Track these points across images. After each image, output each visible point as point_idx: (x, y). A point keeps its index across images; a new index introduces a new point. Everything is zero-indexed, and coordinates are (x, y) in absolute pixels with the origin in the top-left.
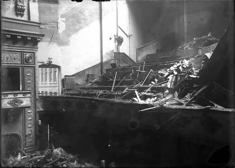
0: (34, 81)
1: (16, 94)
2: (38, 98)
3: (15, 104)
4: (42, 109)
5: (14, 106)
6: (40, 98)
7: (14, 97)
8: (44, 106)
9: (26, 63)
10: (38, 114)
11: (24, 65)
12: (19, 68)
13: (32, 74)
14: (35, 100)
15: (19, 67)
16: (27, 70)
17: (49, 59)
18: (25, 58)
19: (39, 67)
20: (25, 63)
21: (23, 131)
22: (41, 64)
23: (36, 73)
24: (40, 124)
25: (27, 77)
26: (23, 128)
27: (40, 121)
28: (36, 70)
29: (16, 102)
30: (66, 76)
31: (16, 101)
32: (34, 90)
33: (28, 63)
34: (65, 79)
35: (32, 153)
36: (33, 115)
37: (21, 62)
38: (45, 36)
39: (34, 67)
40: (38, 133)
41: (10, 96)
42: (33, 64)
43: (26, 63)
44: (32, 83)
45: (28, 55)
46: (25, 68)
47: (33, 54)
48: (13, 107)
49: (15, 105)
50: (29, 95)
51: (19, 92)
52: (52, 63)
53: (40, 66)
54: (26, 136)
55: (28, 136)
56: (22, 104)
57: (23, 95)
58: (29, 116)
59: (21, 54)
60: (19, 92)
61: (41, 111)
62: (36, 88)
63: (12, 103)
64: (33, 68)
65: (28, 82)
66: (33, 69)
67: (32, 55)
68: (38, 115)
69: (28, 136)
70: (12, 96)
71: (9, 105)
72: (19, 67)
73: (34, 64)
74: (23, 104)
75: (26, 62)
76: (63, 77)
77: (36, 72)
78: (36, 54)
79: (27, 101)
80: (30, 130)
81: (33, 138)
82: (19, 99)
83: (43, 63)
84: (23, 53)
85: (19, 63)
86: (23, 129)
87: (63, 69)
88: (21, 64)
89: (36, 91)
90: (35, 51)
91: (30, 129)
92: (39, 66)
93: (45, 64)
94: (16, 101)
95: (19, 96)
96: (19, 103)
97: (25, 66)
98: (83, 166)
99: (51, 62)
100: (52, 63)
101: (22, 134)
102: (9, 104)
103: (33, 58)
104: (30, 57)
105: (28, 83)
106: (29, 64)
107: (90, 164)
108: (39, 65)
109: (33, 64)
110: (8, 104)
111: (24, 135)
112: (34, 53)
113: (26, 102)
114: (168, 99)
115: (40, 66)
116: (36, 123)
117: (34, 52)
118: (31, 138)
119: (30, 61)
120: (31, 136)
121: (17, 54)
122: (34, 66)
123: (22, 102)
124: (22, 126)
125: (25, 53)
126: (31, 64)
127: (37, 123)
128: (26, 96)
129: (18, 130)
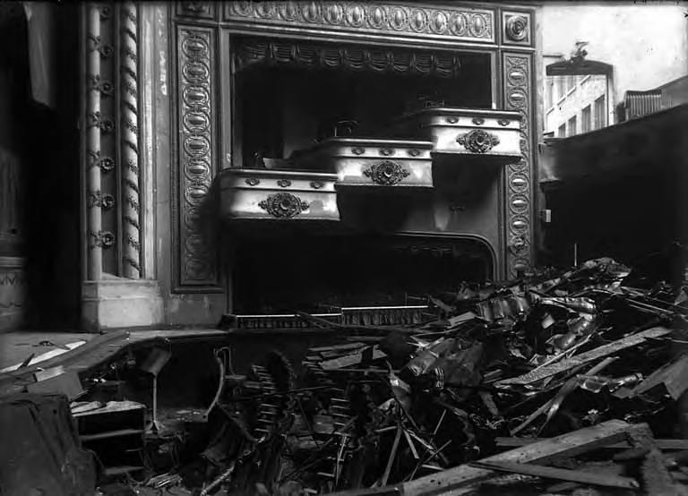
1: (481, 117)
2: (542, 144)
3: (478, 145)
4: (553, 178)
5: (474, 150)
6: (549, 143)
7: (475, 125)
9: (508, 42)
10: (543, 191)
11: (503, 47)
12: (488, 56)
13: (527, 96)
14: (536, 149)
15: (490, 52)
16: (509, 61)
17: (577, 44)
18: (506, 25)
20: (506, 41)
21: (500, 235)
24: (548, 219)
27: (548, 212)
29: (481, 139)
30: (629, 93)
34: (628, 103)
35: (520, 361)
36: (527, 191)
38: (509, 438)
39: (532, 53)
40: (542, 247)
41: (463, 122)
42: (529, 43)
43: (508, 42)
44: (526, 100)
46: (505, 54)
50: (515, 124)
51: (488, 112)
53: (551, 71)
54: (508, 250)
55: (514, 251)
57: (500, 123)
58: (517, 196)
60: (488, 112)
61: (550, 182)
62: (536, 129)
63: (470, 142)
64: (529, 56)
66: (529, 60)
67: (526, 18)
68: (541, 196)
69: (514, 251)
70: (467, 122)
72: (490, 52)
73: (533, 45)
74: (497, 150)
75: (509, 38)
76: (621, 98)
81: (528, 262)
82: (489, 132)
83: (560, 57)
84: (499, 12)
85: (490, 40)
88: (496, 43)
91: (520, 232)
92: (547, 67)
95: (296, 185)
96: (487, 143)
97: (506, 51)
98: (585, 325)
99: (585, 53)
100: (587, 58)
102: (461, 144)
103: (528, 28)
105: (514, 99)
108: (548, 64)
109: (529, 43)
111: (503, 247)
113: (508, 142)
115: (551, 71)
116: (537, 219)
118: (521, 258)
119: (522, 34)
121: (484, 16)
122: (530, 49)
123: (496, 143)
124: (496, 221)
125: (505, 13)
126: (525, 43)
127: (540, 217)
128: (507, 127)
129: (484, 229)
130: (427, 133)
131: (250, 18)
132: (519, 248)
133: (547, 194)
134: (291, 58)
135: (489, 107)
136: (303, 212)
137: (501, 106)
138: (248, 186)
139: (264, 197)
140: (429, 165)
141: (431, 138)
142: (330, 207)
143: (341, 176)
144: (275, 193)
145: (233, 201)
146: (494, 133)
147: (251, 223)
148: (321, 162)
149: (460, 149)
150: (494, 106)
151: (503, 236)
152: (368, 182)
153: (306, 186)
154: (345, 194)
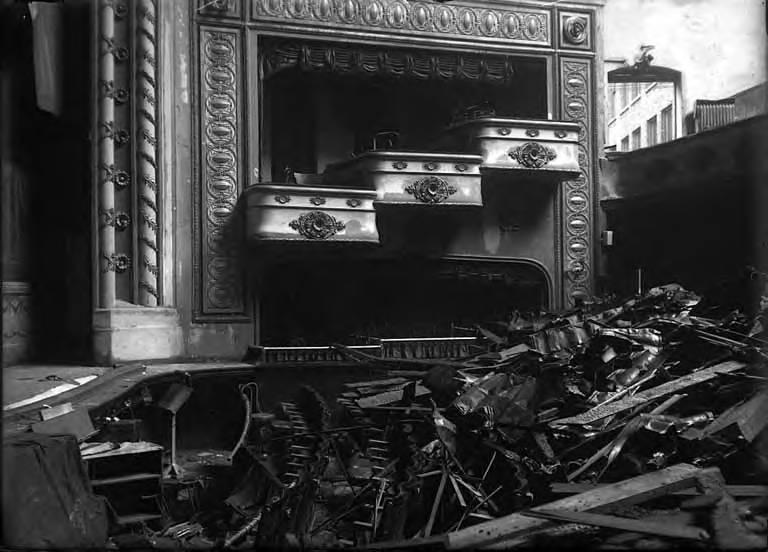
0: (591, 177)
1: (536, 129)
2: (603, 158)
6: (612, 158)
8: (621, 185)
9: (563, 45)
12: (544, 61)
17: (642, 48)
19: (610, 81)
21: (556, 260)
22: (613, 67)
23: (598, 79)
24: (610, 242)
25: (571, 113)
26: (556, 247)
27: (610, 233)
28: (597, 69)
30: (700, 102)
31: (532, 150)
32: (592, 111)
33: (572, 43)
34: (698, 113)
37: (549, 40)
39: (592, 58)
42: (589, 47)
45: (574, 17)
46: (562, 59)
47: (587, 16)
48: (524, 168)
49: (530, 162)
50: (574, 137)
52: (652, 63)
53: (613, 77)
54: (565, 275)
55: (572, 277)
56: (551, 163)
58: (576, 216)
59: (554, 58)
63: (306, 227)
64: (588, 61)
65: (572, 105)
67: (585, 19)
68: (601, 213)
69: (572, 277)
70: (520, 134)
71: (515, 162)
73: (593, 49)
75: (567, 40)
76: (691, 108)
77: (598, 74)
78: (599, 17)
79: (569, 154)
80: (577, 254)
82: (545, 145)
83: (622, 62)
85: (545, 44)
86: (556, 253)
87: (688, 82)
89: (596, 136)
90: (594, 8)
93: (628, 67)
94: (532, 150)
95: (545, 135)
96: (543, 157)
100: (652, 63)
101: (553, 269)
102: (513, 158)
103: (588, 29)
104: (578, 27)
106: (581, 46)
107: (754, 395)
110: (510, 158)
112: (591, 13)
113: (565, 157)
114: (621, 402)
115: (613, 77)
117: (592, 11)
119: (581, 37)
120: (583, 279)
123: (552, 157)
125: (562, 14)
126: (581, 46)
129: (539, 252)
130: (476, 146)
131: (281, 18)
132: (577, 274)
133: (609, 214)
134: (326, 62)
135: (546, 119)
136: (339, 233)
137: (558, 117)
138: (278, 204)
139: (295, 216)
140: (478, 181)
141: (481, 152)
142: (369, 227)
143: (381, 193)
144: (307, 212)
145: (260, 220)
146: (551, 146)
147: (282, 245)
148: (357, 177)
149: (513, 163)
150: (550, 116)
151: (560, 260)
152: (411, 199)
153: (341, 204)
154: (386, 213)
